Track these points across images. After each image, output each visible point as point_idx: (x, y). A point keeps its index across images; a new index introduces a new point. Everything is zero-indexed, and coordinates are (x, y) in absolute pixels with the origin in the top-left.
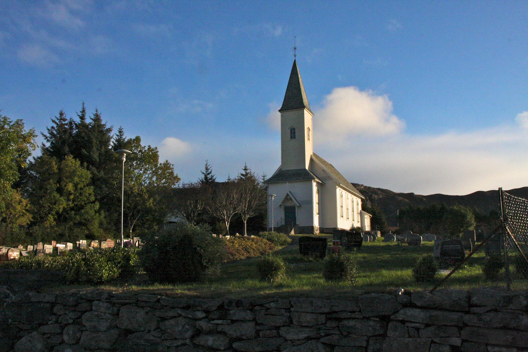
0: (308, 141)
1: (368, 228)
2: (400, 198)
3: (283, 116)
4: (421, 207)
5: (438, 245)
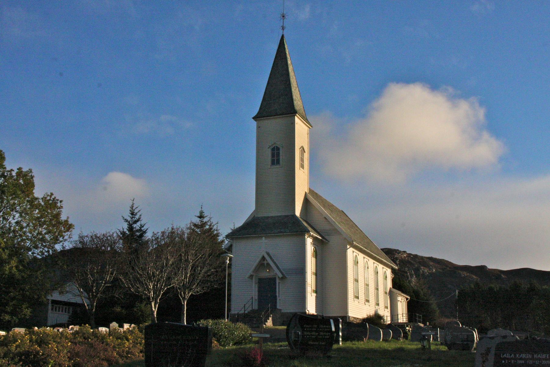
0: (301, 169)
1: (402, 318)
2: (465, 273)
4: (495, 286)
5: (488, 351)
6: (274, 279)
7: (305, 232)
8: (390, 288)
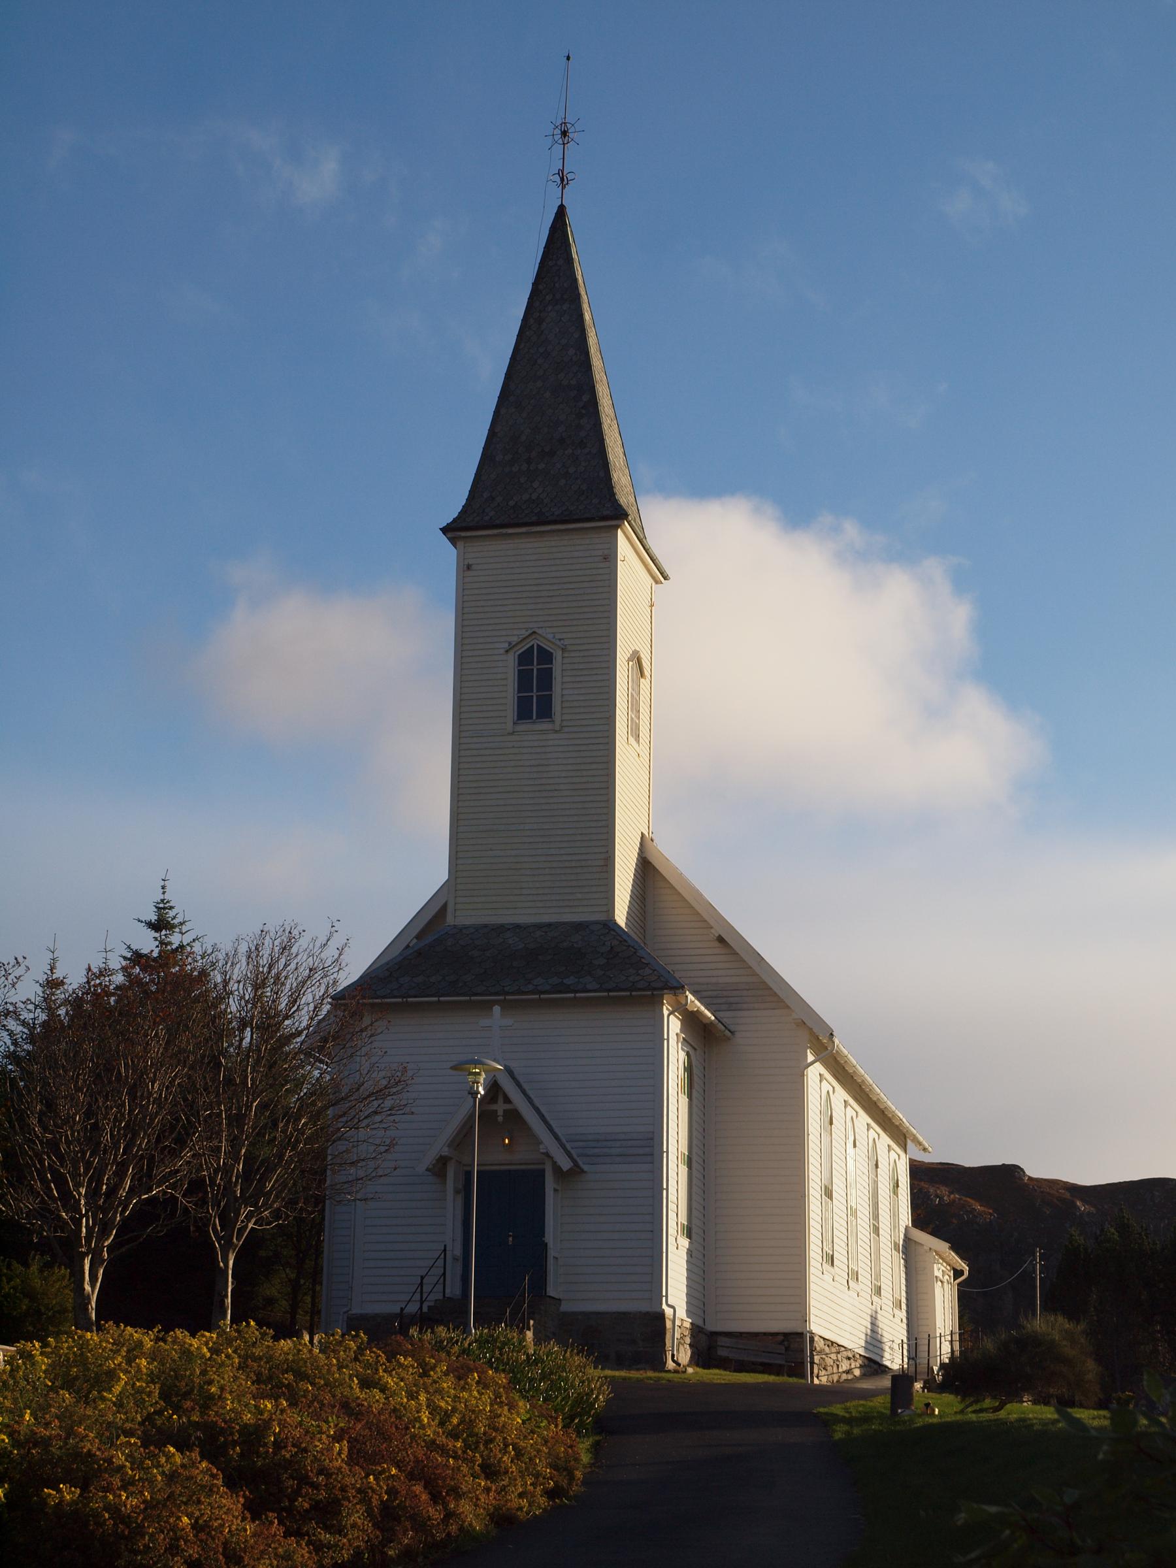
2: (944, 1191)
3: (469, 567)
6: (538, 1177)
7: (662, 989)
8: (907, 1228)
